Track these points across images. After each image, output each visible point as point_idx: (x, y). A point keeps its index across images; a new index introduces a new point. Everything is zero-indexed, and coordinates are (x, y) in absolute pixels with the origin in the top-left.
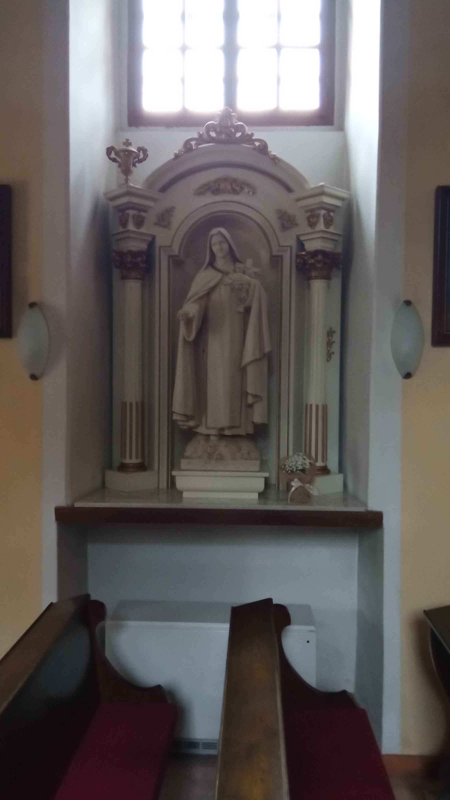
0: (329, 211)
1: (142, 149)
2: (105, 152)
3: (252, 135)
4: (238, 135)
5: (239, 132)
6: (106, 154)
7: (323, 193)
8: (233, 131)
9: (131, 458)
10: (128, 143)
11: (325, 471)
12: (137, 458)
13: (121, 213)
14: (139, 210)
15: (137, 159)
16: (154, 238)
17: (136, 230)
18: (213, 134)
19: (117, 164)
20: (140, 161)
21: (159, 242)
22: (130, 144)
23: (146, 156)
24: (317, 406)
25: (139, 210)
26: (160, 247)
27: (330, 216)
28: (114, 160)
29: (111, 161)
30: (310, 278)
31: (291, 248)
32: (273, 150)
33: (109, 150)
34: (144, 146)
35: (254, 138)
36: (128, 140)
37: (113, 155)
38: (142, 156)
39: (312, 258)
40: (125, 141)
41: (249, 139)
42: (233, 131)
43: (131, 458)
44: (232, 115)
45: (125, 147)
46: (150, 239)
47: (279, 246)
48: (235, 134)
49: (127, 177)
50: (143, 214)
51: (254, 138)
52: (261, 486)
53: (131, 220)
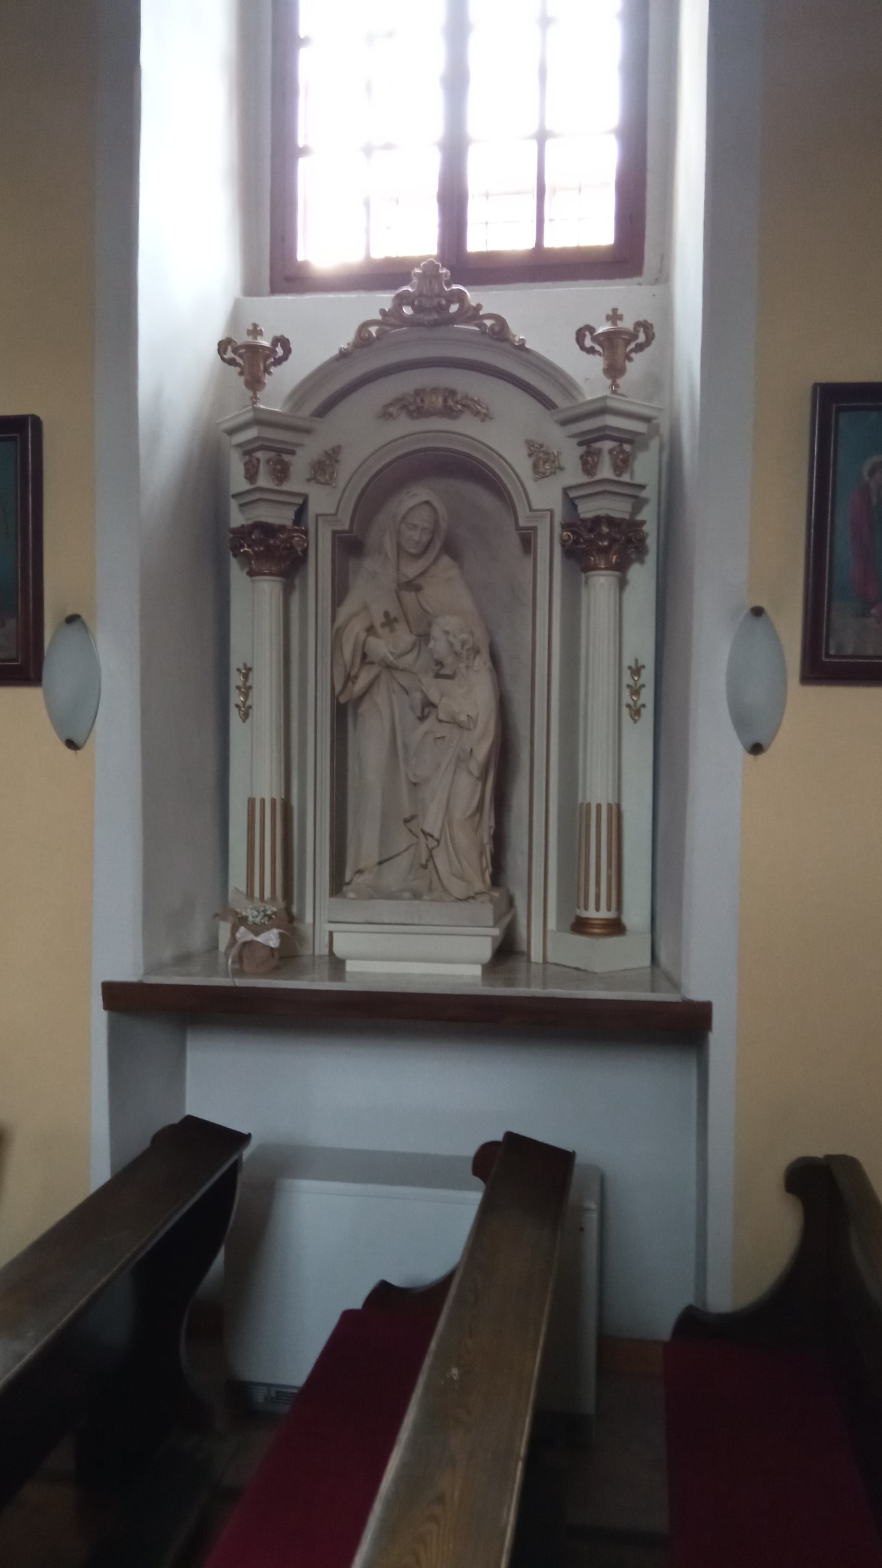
0: (621, 441)
1: (282, 341)
2: (216, 347)
3: (479, 307)
4: (454, 308)
5: (453, 302)
6: (217, 352)
7: (604, 411)
8: (444, 302)
9: (598, 909)
10: (255, 331)
11: (615, 927)
12: (609, 909)
13: (247, 458)
14: (621, 441)
15: (272, 360)
16: (306, 498)
17: (616, 478)
18: (407, 311)
19: (238, 369)
20: (279, 362)
21: (313, 509)
22: (620, 318)
23: (288, 351)
24: (599, 806)
25: (279, 451)
26: (317, 516)
27: (622, 451)
28: (231, 362)
29: (227, 365)
30: (588, 568)
31: (552, 512)
32: (518, 331)
33: (222, 346)
34: (638, 320)
35: (481, 313)
36: (255, 326)
37: (229, 355)
38: (280, 351)
39: (591, 530)
40: (611, 313)
41: (473, 314)
42: (444, 302)
43: (598, 909)
44: (441, 273)
45: (249, 339)
46: (300, 501)
47: (531, 510)
48: (448, 307)
49: (255, 394)
50: (286, 457)
51: (481, 313)
52: (486, 951)
53: (262, 468)
